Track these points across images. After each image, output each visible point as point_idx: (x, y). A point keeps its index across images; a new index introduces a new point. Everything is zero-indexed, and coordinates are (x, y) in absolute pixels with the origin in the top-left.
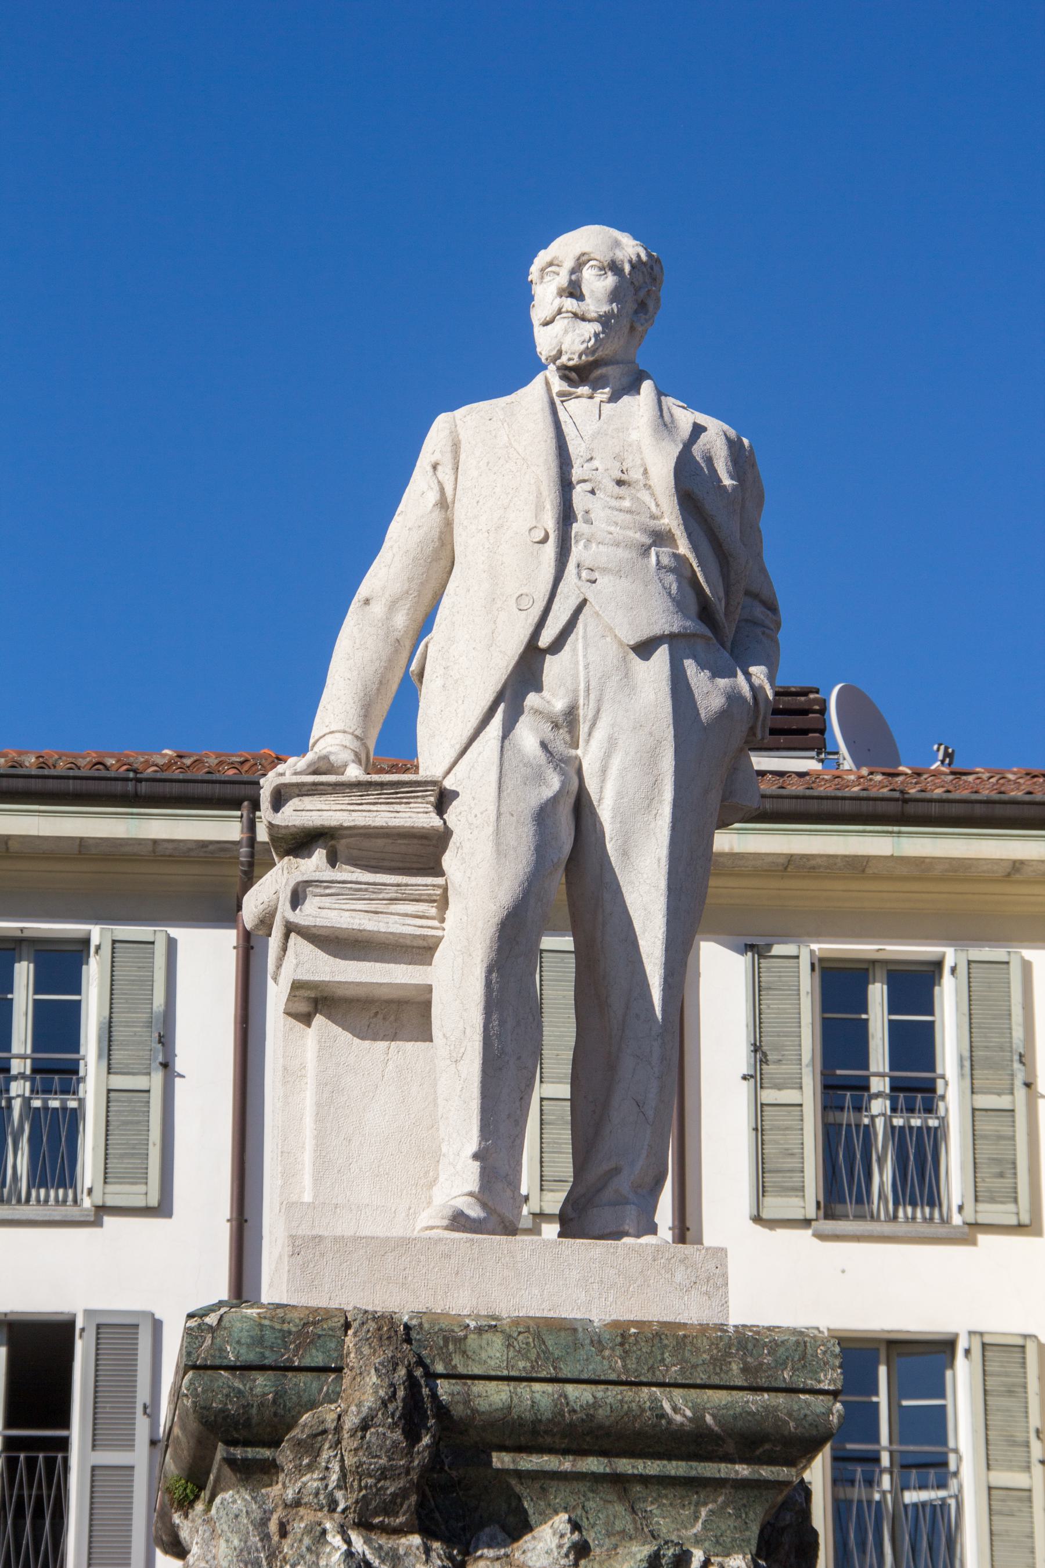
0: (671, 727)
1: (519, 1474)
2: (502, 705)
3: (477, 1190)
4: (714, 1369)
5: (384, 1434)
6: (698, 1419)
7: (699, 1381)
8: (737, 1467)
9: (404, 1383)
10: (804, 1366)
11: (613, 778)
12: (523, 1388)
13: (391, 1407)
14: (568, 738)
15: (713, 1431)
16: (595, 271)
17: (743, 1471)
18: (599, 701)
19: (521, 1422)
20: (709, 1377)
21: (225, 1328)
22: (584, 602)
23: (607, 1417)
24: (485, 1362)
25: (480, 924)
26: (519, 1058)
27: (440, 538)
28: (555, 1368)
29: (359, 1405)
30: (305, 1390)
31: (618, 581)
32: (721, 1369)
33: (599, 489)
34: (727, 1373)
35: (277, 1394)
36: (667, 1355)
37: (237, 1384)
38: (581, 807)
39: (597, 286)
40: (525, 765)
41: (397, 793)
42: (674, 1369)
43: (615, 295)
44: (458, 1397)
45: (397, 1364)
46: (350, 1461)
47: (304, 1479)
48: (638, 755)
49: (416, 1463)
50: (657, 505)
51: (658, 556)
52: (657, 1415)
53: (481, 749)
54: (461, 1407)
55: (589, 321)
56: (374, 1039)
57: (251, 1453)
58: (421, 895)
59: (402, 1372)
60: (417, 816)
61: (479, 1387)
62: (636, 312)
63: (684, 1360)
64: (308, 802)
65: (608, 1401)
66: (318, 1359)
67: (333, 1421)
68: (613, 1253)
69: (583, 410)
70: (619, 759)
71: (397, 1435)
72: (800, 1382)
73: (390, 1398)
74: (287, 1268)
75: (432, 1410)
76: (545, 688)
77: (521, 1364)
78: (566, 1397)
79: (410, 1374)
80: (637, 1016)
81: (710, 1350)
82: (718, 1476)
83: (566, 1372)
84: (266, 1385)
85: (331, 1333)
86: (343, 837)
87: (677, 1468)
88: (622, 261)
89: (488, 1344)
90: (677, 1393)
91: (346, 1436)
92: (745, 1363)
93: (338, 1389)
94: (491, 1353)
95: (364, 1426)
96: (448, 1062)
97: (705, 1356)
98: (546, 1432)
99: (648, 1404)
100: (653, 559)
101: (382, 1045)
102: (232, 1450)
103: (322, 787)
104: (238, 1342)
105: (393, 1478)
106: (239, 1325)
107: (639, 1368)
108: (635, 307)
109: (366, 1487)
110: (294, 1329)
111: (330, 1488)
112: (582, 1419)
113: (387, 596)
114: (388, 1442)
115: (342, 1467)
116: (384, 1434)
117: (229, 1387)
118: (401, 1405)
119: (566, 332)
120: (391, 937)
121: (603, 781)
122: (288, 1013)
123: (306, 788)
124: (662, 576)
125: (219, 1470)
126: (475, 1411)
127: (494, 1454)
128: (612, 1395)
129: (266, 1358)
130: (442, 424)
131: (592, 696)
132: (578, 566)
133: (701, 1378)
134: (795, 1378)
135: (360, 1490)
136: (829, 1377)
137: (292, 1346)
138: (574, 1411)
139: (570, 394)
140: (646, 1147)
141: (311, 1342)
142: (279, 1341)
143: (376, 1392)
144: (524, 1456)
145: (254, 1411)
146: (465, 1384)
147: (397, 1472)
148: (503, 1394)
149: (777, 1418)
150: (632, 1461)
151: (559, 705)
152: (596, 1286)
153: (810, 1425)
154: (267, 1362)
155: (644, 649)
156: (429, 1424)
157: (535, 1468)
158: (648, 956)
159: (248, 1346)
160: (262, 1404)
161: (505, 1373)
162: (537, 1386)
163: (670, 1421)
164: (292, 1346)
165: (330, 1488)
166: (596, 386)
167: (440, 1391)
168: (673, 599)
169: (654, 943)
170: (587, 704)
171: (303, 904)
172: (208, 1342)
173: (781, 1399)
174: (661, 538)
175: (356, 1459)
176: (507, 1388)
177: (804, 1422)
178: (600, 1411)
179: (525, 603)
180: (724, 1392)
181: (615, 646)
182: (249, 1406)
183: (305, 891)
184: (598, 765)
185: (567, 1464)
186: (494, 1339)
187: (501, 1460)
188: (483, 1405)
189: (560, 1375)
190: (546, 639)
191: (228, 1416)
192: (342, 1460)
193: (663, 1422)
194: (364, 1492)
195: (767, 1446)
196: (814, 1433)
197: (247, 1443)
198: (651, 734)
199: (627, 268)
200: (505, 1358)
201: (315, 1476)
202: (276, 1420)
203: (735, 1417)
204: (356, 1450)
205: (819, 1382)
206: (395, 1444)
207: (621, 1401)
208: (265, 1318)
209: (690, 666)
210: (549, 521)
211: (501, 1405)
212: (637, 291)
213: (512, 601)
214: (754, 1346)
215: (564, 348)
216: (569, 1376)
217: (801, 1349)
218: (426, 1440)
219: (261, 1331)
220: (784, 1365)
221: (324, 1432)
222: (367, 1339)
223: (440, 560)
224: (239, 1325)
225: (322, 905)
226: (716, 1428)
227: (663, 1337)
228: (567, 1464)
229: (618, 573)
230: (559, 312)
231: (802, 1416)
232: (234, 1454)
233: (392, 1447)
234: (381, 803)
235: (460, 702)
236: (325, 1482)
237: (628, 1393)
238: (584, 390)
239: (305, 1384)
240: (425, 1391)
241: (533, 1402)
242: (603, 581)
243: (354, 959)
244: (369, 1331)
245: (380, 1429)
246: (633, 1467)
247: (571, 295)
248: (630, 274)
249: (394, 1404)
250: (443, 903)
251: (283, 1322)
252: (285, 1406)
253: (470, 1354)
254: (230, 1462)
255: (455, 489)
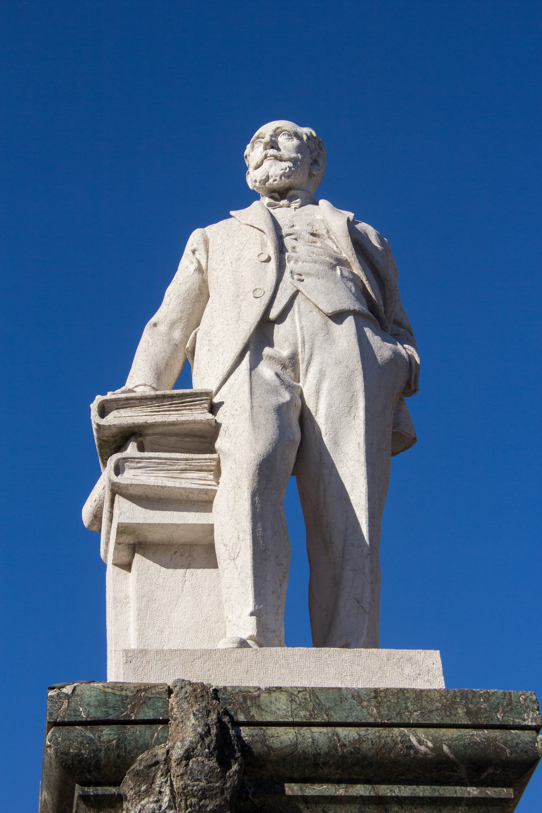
0: (360, 362)
1: (306, 799)
2: (248, 353)
3: (255, 634)
4: (445, 713)
5: (203, 762)
6: (437, 749)
7: (435, 722)
8: (469, 789)
9: (216, 724)
10: (511, 710)
11: (324, 395)
12: (304, 730)
13: (207, 741)
14: (292, 375)
15: (449, 758)
16: (286, 137)
17: (473, 791)
18: (312, 348)
19: (305, 756)
20: (442, 719)
21: (78, 696)
22: (297, 292)
23: (369, 749)
24: (275, 713)
25: (245, 466)
26: (277, 557)
27: (199, 289)
28: (327, 715)
29: (182, 741)
30: (140, 736)
31: (317, 280)
32: (451, 713)
33: (300, 238)
34: (455, 715)
35: (119, 740)
36: (409, 704)
37: (89, 734)
38: (305, 418)
39: (288, 146)
40: (266, 384)
41: (182, 403)
42: (415, 714)
43: (299, 149)
44: (257, 737)
45: (210, 711)
46: (177, 784)
47: (143, 802)
48: (340, 380)
49: (228, 784)
50: (337, 247)
51: (341, 271)
52: (406, 747)
53: (236, 377)
54: (259, 745)
55: (285, 161)
56: (175, 567)
57: (100, 790)
58: (202, 466)
59: (214, 716)
60: (199, 415)
61: (272, 731)
62: (311, 164)
63: (422, 708)
64: (123, 413)
65: (369, 737)
66: (150, 714)
67: (163, 754)
68: (358, 656)
69: (285, 214)
70: (327, 384)
71: (213, 763)
72: (511, 720)
73: (206, 733)
74: (122, 672)
75: (237, 746)
76: (275, 345)
77: (302, 713)
78: (337, 735)
79: (219, 720)
80: (353, 545)
81: (441, 700)
82: (455, 796)
83: (336, 718)
84: (110, 734)
85: (158, 696)
86: (147, 436)
87: (424, 791)
88: (302, 134)
89: (276, 700)
90: (421, 732)
91: (174, 765)
92: (468, 708)
93: (166, 735)
94: (279, 706)
95: (188, 756)
96: (229, 561)
97: (437, 704)
98: (324, 764)
99: (399, 738)
100: (338, 272)
101: (181, 571)
102: (86, 789)
103: (132, 401)
104: (88, 705)
105: (211, 798)
106: (88, 693)
107: (390, 714)
108: (312, 161)
109: (191, 806)
110: (130, 694)
111: (163, 808)
112: (351, 752)
113: (168, 320)
114: (206, 768)
115: (172, 791)
116: (203, 762)
117: (82, 736)
118: (215, 738)
119: (271, 166)
120: (183, 492)
121: (318, 399)
122: (113, 564)
123: (122, 403)
124: (345, 281)
125: (78, 805)
126: (270, 748)
127: (286, 785)
128: (372, 732)
129: (109, 715)
130: (195, 238)
131: (307, 346)
132: (291, 272)
133: (436, 719)
134: (506, 718)
135: (186, 809)
136: (531, 717)
137: (129, 706)
138: (345, 745)
139: (276, 205)
140: (366, 629)
141: (144, 703)
142: (119, 703)
143: (195, 730)
144: (308, 785)
145: (102, 754)
146: (262, 729)
147: (214, 792)
148: (290, 734)
149: (496, 747)
150: (389, 786)
151: (285, 353)
152: (348, 678)
153: (522, 751)
154: (110, 717)
155: (338, 317)
156: (237, 756)
157: (317, 794)
158: (357, 505)
159: (96, 707)
160: (108, 749)
161: (291, 719)
162: (315, 729)
163: (417, 751)
164: (129, 706)
165: (163, 808)
166: (291, 199)
167: (243, 734)
168: (354, 294)
169: (360, 496)
170: (303, 351)
171: (123, 473)
172: (65, 705)
173: (497, 733)
174: (341, 262)
175: (182, 783)
176: (293, 731)
177: (516, 748)
178: (364, 745)
179: (258, 294)
180: (455, 730)
181: (319, 317)
182: (99, 750)
183: (123, 465)
184: (313, 388)
185: (341, 791)
186: (281, 696)
187: (292, 789)
188: (275, 743)
189: (332, 720)
190: (274, 313)
191: (82, 759)
192: (172, 785)
193: (412, 752)
194: (189, 810)
195: (490, 770)
196: (525, 757)
197: (97, 784)
198: (347, 367)
199: (305, 138)
200: (289, 709)
201: (151, 800)
202: (119, 761)
203: (465, 747)
204: (182, 775)
205: (524, 720)
206: (212, 770)
207: (379, 737)
208: (108, 687)
209: (368, 332)
210: (271, 250)
211: (289, 743)
212: (311, 152)
213: (251, 295)
214: (473, 696)
215: (270, 174)
216: (339, 720)
217: (508, 697)
218: (235, 767)
219: (106, 696)
220: (496, 709)
221: (157, 763)
222: (186, 698)
223: (201, 296)
224: (88, 693)
225: (136, 474)
226: (452, 756)
227: (405, 692)
228: (341, 791)
229: (317, 276)
230: (266, 157)
231: (515, 745)
232: (88, 792)
233: (210, 772)
234: (172, 411)
235: (220, 355)
236: (159, 803)
237: (384, 732)
238: (284, 202)
239: (140, 732)
240: (232, 732)
241: (313, 739)
242: (308, 280)
243: (159, 510)
244: (186, 692)
245: (200, 758)
246: (391, 791)
247: (272, 148)
248: (307, 141)
249: (210, 738)
250: (217, 472)
251: (122, 690)
252: (126, 749)
253: (263, 707)
254: (85, 798)
255: (207, 262)
